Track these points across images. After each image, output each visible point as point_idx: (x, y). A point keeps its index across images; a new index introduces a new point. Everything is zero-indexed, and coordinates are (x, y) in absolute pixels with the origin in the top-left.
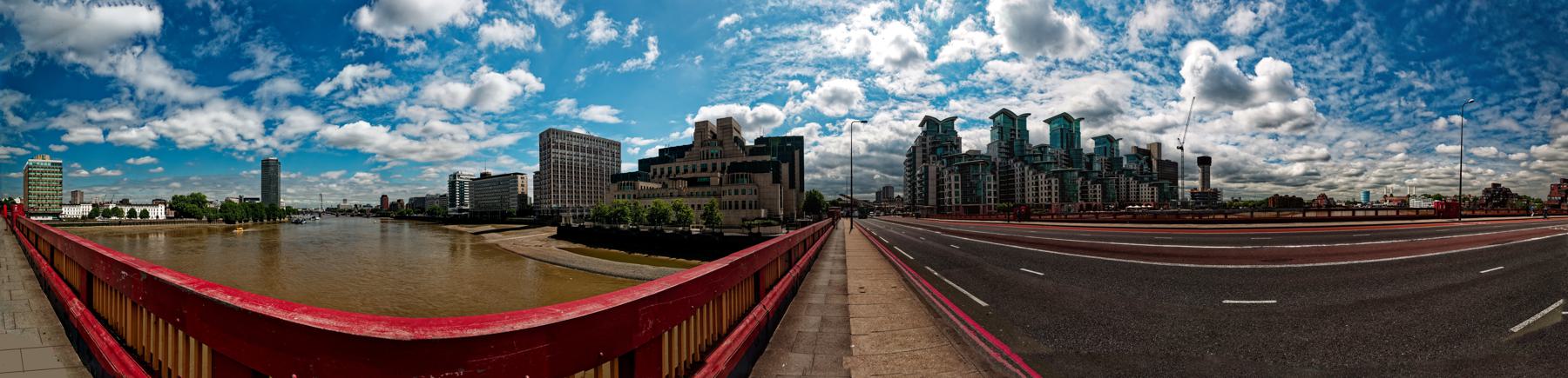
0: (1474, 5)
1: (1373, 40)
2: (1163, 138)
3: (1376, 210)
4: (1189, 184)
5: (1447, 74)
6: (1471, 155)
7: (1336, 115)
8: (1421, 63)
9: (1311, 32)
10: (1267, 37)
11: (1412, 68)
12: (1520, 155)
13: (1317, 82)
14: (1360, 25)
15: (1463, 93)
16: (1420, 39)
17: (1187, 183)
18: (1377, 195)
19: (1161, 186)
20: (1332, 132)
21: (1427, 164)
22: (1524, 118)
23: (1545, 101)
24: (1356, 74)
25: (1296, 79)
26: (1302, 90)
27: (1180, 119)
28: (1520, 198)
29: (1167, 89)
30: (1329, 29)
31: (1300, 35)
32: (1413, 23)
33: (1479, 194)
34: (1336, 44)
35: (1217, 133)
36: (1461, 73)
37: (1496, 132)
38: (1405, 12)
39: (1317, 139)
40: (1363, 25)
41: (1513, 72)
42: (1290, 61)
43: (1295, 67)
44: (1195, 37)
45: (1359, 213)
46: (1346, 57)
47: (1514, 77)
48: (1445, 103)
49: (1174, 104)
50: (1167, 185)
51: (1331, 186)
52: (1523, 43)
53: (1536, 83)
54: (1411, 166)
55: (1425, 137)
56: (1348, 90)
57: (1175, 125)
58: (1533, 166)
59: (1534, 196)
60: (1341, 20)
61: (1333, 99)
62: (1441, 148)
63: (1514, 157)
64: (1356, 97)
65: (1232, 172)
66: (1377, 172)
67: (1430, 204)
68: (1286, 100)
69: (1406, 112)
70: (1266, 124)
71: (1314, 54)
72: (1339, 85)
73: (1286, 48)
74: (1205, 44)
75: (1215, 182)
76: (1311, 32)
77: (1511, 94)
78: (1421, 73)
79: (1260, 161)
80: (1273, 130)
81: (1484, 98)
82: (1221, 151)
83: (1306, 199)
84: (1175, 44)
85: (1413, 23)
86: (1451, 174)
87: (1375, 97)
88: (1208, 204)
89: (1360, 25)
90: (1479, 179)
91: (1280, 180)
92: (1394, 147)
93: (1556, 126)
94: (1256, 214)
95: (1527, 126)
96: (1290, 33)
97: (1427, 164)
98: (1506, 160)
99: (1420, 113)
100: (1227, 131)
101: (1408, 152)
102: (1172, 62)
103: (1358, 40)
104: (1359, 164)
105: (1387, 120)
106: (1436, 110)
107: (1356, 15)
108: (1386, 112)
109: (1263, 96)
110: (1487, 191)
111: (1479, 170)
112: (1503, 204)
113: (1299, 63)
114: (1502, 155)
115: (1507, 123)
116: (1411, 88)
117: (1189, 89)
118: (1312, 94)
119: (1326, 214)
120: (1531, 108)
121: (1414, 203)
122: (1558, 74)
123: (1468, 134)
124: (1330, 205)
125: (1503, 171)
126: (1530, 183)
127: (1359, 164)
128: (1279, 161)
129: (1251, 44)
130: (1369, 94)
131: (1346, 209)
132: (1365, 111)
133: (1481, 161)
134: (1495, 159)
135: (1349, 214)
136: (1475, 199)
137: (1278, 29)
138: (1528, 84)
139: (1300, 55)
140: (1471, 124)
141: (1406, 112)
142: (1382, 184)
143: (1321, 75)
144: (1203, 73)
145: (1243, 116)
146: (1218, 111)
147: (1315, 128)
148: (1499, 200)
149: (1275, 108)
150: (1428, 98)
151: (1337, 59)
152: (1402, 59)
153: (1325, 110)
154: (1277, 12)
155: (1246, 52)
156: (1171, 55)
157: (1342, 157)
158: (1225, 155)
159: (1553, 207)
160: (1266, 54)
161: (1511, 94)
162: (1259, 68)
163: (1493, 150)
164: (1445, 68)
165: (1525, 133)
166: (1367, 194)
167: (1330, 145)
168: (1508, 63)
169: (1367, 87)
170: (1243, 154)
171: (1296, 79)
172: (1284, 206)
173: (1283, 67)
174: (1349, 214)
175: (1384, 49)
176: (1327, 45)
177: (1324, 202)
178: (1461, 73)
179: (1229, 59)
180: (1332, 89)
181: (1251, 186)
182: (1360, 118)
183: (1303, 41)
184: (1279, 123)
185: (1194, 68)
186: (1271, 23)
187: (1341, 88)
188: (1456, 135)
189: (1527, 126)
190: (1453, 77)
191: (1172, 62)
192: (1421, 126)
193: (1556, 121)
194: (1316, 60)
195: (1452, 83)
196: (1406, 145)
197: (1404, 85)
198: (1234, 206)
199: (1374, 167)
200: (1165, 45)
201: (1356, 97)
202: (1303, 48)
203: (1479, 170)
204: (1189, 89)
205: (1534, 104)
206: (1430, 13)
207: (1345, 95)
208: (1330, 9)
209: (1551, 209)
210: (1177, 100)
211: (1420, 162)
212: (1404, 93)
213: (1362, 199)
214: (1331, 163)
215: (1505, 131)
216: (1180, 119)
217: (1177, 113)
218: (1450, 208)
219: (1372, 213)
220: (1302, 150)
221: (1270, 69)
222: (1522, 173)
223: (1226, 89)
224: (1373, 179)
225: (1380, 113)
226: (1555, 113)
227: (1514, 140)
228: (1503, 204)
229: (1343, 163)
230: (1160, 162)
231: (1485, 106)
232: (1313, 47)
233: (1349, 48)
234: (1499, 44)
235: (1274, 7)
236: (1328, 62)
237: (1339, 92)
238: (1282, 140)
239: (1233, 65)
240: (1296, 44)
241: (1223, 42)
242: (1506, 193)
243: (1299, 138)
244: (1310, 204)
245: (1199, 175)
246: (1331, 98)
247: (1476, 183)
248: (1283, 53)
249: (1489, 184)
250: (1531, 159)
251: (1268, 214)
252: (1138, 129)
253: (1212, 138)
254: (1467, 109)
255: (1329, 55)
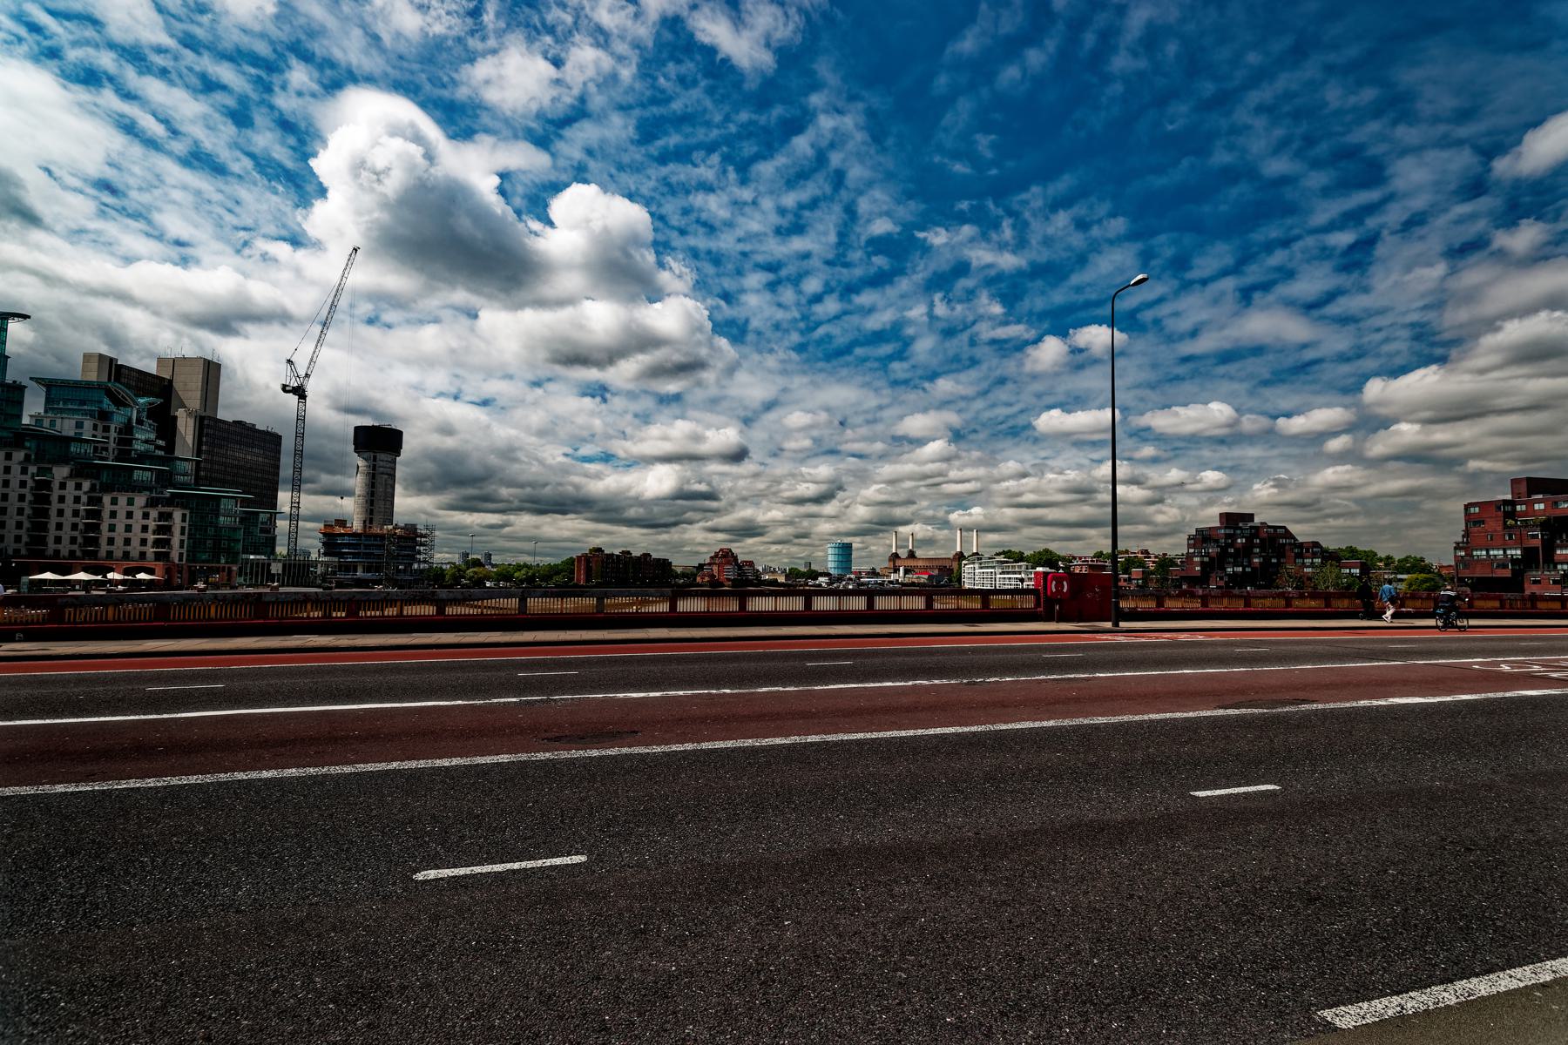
0: (1138, 19)
1: (860, 157)
2: (228, 349)
3: (870, 594)
4: (313, 510)
5: (1062, 219)
6: (1144, 435)
7: (763, 344)
8: (987, 202)
9: (701, 134)
10: (584, 133)
11: (962, 219)
12: (1323, 416)
13: (716, 259)
14: (826, 123)
15: (1113, 263)
16: (984, 142)
17: (310, 502)
18: (872, 554)
19: (203, 510)
20: (752, 387)
21: (1011, 466)
22: (1331, 297)
23: (1414, 223)
24: (817, 241)
25: (661, 247)
26: (675, 276)
27: (304, 301)
28: (1332, 557)
29: (261, 201)
30: (747, 131)
31: (673, 140)
32: (965, 106)
33: (1176, 546)
34: (766, 169)
35: (427, 362)
36: (1104, 208)
37: (1228, 357)
38: (942, 82)
39: (713, 403)
40: (833, 122)
41: (1277, 167)
42: (647, 202)
43: (659, 218)
44: (370, 80)
45: (822, 604)
46: (790, 200)
47: (1284, 180)
48: (1059, 297)
49: (282, 250)
50: (231, 504)
51: (749, 530)
52: (1310, 69)
53: (1374, 173)
54: (965, 474)
55: (1002, 394)
56: (796, 280)
57: (279, 317)
58: (1379, 446)
59: (1385, 548)
60: (778, 111)
61: (755, 304)
62: (1051, 420)
63: (1298, 424)
64: (817, 299)
65: (464, 479)
66: (872, 492)
67: (1026, 577)
68: (632, 299)
69: (949, 332)
70: (574, 356)
71: (708, 188)
72: (772, 267)
73: (636, 168)
74: (404, 110)
75: (408, 504)
76: (701, 134)
77: (1274, 232)
78: (987, 226)
79: (554, 454)
80: (593, 374)
81: (1180, 264)
82: (432, 417)
83: (679, 562)
84: (299, 75)
85: (965, 106)
86: (1083, 492)
87: (865, 298)
88: (381, 570)
89: (826, 123)
90: (1176, 504)
91: (608, 510)
92: (915, 424)
93: (1471, 296)
94: (536, 604)
95: (1345, 320)
96: (647, 132)
97: (1011, 466)
98: (1269, 436)
99: (986, 332)
100: (457, 361)
101: (957, 436)
102: (286, 125)
103: (821, 158)
104: (824, 470)
105: (900, 356)
106: (1034, 318)
107: (816, 100)
108: (896, 337)
109: (570, 282)
110: (1202, 538)
111: (1174, 475)
112: (1266, 577)
113: (670, 207)
114: (1250, 423)
115: (1267, 324)
116: (962, 269)
117: (339, 216)
118: (701, 287)
119: (732, 606)
120: (1358, 259)
121: (974, 577)
122: (1464, 115)
123: (1130, 372)
124: (746, 581)
125: (1259, 472)
126: (1368, 506)
127: (824, 470)
128: (607, 458)
129: (542, 142)
130: (850, 290)
131: (788, 591)
132: (840, 334)
133: (1178, 447)
134: (1230, 438)
135: (797, 604)
136: (1165, 563)
137: (617, 120)
138: (1344, 186)
139: (671, 188)
140: (1142, 344)
141: (949, 332)
142: (883, 524)
143: (726, 243)
144: (393, 185)
145: (507, 329)
146: (433, 303)
147: (708, 376)
148: (1246, 563)
149: (601, 317)
150: (1010, 289)
151: (767, 204)
152: (935, 198)
153: (735, 330)
154: (613, 78)
155: (524, 158)
156: (283, 102)
157: (777, 453)
158: (447, 430)
159: (1485, 586)
160: (581, 174)
161: (1274, 232)
162: (559, 207)
163: (1219, 411)
164: (1056, 205)
165: (1339, 341)
166: (846, 551)
167: (747, 422)
168: (1256, 146)
169: (845, 274)
170: (503, 432)
171: (661, 247)
172: (620, 582)
173: (626, 214)
174: (796, 604)
175: (890, 176)
176: (744, 170)
177: (729, 573)
178: (1104, 208)
179: (477, 168)
180: (755, 279)
181: (524, 522)
182: (824, 353)
183: (682, 155)
184: (610, 356)
185: (359, 166)
186: (597, 101)
187: (777, 275)
188: (1096, 380)
189: (1345, 320)
190: (1082, 225)
191: (286, 125)
192: (993, 365)
193: (1473, 275)
194: (714, 206)
195: (1077, 240)
196: (952, 418)
197: (942, 263)
198: (470, 578)
199: (863, 478)
200: (266, 68)
201: (817, 299)
202: (679, 172)
203: (1174, 475)
204: (339, 216)
205: (1367, 244)
206: (1010, 74)
207: (788, 295)
208: (751, 85)
209: (1449, 596)
210: (296, 240)
211: (990, 460)
212: (941, 282)
213: (831, 566)
214: (747, 467)
215: (1258, 350)
216: (304, 301)
217: (294, 280)
218: (1081, 592)
219: (859, 604)
220: (673, 432)
221: (585, 216)
222: (1332, 474)
223: (455, 246)
224: (862, 512)
225: (878, 337)
226: (1462, 251)
227: (1296, 371)
228: (1266, 577)
229: (780, 468)
230: (208, 425)
231: (1186, 286)
232: (706, 172)
233: (797, 177)
234: (1223, 101)
235: (607, 62)
236: (746, 212)
237: (772, 287)
238: (617, 403)
239: (485, 185)
240: (663, 159)
241: (461, 118)
242: (1276, 542)
243: (665, 400)
244: (690, 575)
245: (357, 482)
246: (752, 300)
247: (1166, 514)
248: (629, 180)
249: (1210, 516)
250: (1371, 423)
251: (570, 605)
252: (124, 297)
253: (410, 375)
254: (1126, 303)
255: (746, 194)
